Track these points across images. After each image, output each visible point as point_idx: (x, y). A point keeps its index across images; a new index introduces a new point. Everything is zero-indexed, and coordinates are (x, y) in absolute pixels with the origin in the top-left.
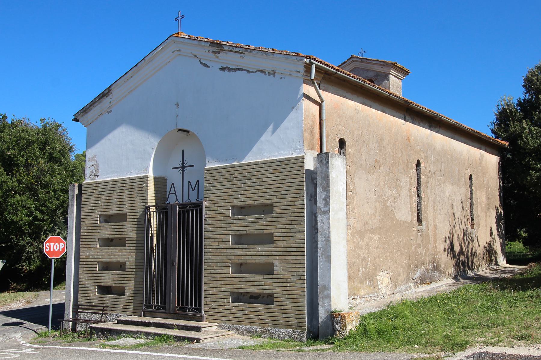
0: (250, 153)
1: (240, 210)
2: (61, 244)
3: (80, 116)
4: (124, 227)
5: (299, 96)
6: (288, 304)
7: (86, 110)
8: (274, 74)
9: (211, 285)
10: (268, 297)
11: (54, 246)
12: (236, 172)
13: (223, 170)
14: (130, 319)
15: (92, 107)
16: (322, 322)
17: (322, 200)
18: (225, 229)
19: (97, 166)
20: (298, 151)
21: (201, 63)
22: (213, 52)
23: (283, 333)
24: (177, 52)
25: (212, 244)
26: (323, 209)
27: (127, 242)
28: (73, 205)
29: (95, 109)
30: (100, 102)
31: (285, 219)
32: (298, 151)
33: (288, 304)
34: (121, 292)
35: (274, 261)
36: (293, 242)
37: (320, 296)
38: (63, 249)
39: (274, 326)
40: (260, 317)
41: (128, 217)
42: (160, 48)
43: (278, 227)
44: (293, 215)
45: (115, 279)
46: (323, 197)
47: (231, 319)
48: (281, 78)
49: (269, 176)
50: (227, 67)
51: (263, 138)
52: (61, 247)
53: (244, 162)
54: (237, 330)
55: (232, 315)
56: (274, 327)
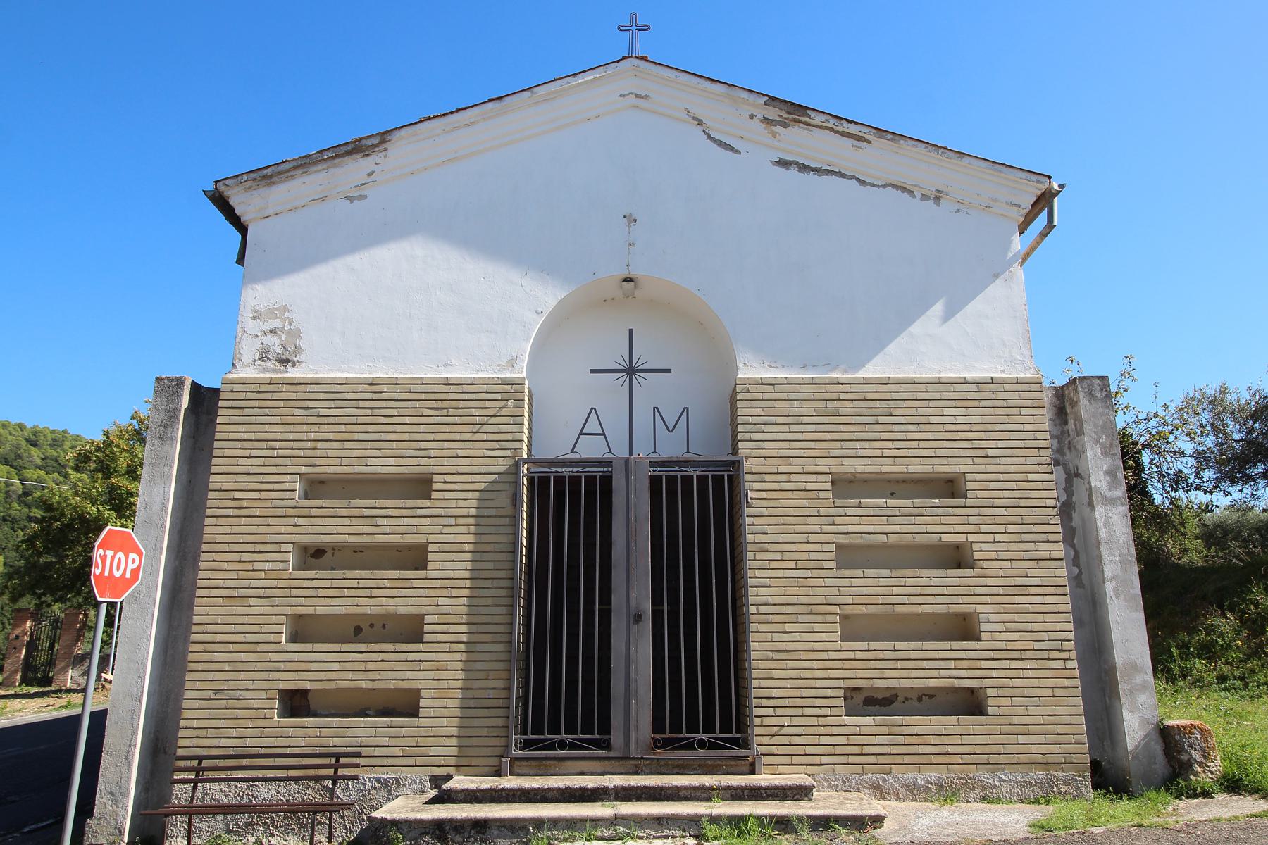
0: (881, 354)
1: (846, 486)
2: (132, 556)
3: (240, 188)
4: (420, 512)
5: (1010, 255)
6: (1032, 710)
7: (271, 176)
8: (937, 199)
9: (776, 674)
10: (920, 699)
11: (113, 558)
12: (842, 396)
13: (804, 388)
14: (510, 782)
15: (299, 172)
16: (1137, 747)
17: (1102, 473)
18: (817, 529)
19: (296, 334)
20: (1018, 367)
21: (709, 137)
22: (765, 120)
23: (1024, 785)
24: (632, 100)
25: (774, 565)
26: (1108, 494)
27: (431, 556)
28: (173, 439)
29: (308, 179)
30: (335, 166)
31: (1003, 511)
32: (1018, 367)
33: (1032, 710)
34: (404, 706)
35: (980, 609)
36: (1033, 564)
37: (1123, 687)
38: (135, 572)
39: (994, 768)
40: (951, 749)
41: (435, 486)
42: (590, 76)
43: (984, 528)
44: (1023, 503)
45: (371, 666)
46: (1105, 467)
47: (852, 759)
48: (958, 211)
49: (946, 412)
50: (796, 163)
51: (916, 328)
52: (131, 566)
53: (874, 369)
54: (875, 786)
55: (856, 750)
56: (994, 772)
